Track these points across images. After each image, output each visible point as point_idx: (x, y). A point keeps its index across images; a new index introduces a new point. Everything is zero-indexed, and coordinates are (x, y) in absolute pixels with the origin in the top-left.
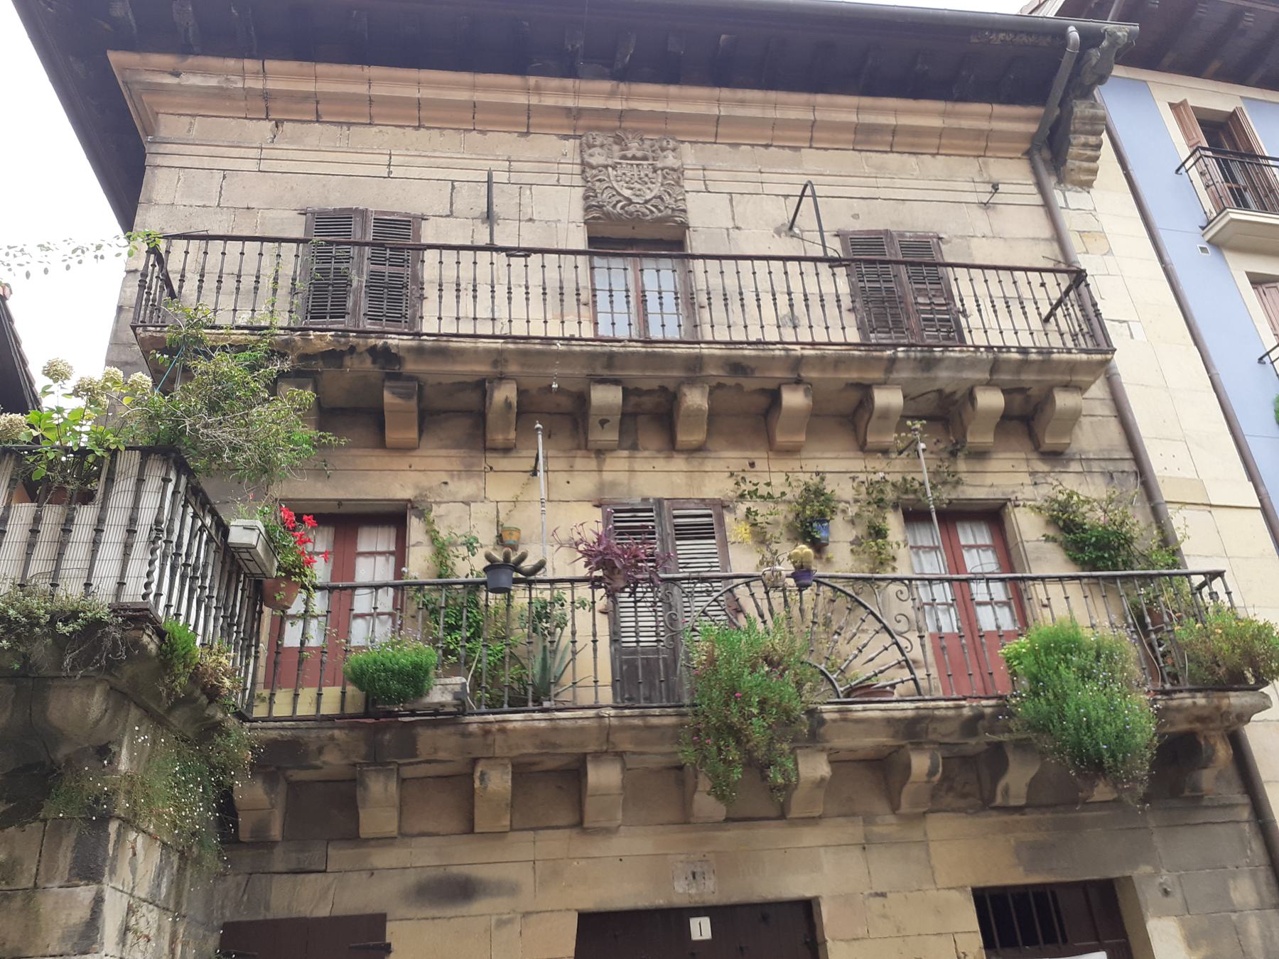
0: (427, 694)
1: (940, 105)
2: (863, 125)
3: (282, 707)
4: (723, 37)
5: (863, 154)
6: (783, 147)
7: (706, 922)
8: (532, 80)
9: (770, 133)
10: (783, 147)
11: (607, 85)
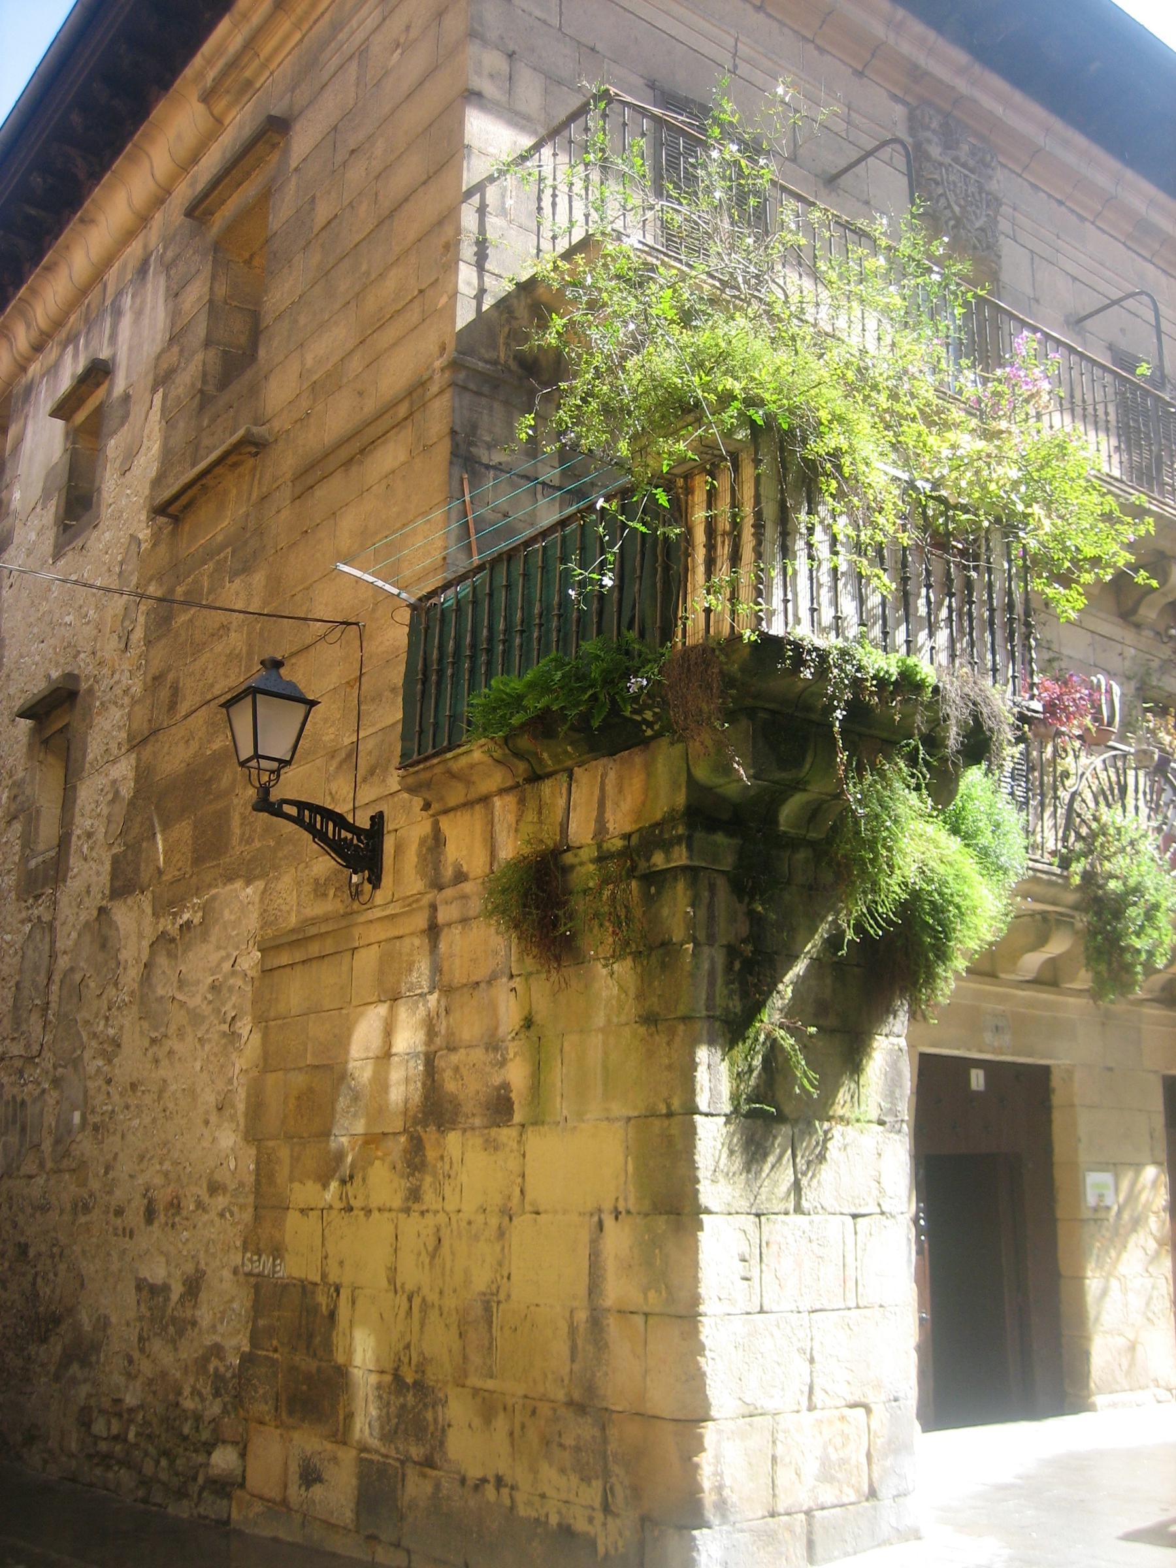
2: (690, 1132)
3: (215, 746)
5: (1130, 253)
6: (1072, 211)
8: (901, 13)
9: (1157, 246)
10: (1072, 211)
11: (961, 57)
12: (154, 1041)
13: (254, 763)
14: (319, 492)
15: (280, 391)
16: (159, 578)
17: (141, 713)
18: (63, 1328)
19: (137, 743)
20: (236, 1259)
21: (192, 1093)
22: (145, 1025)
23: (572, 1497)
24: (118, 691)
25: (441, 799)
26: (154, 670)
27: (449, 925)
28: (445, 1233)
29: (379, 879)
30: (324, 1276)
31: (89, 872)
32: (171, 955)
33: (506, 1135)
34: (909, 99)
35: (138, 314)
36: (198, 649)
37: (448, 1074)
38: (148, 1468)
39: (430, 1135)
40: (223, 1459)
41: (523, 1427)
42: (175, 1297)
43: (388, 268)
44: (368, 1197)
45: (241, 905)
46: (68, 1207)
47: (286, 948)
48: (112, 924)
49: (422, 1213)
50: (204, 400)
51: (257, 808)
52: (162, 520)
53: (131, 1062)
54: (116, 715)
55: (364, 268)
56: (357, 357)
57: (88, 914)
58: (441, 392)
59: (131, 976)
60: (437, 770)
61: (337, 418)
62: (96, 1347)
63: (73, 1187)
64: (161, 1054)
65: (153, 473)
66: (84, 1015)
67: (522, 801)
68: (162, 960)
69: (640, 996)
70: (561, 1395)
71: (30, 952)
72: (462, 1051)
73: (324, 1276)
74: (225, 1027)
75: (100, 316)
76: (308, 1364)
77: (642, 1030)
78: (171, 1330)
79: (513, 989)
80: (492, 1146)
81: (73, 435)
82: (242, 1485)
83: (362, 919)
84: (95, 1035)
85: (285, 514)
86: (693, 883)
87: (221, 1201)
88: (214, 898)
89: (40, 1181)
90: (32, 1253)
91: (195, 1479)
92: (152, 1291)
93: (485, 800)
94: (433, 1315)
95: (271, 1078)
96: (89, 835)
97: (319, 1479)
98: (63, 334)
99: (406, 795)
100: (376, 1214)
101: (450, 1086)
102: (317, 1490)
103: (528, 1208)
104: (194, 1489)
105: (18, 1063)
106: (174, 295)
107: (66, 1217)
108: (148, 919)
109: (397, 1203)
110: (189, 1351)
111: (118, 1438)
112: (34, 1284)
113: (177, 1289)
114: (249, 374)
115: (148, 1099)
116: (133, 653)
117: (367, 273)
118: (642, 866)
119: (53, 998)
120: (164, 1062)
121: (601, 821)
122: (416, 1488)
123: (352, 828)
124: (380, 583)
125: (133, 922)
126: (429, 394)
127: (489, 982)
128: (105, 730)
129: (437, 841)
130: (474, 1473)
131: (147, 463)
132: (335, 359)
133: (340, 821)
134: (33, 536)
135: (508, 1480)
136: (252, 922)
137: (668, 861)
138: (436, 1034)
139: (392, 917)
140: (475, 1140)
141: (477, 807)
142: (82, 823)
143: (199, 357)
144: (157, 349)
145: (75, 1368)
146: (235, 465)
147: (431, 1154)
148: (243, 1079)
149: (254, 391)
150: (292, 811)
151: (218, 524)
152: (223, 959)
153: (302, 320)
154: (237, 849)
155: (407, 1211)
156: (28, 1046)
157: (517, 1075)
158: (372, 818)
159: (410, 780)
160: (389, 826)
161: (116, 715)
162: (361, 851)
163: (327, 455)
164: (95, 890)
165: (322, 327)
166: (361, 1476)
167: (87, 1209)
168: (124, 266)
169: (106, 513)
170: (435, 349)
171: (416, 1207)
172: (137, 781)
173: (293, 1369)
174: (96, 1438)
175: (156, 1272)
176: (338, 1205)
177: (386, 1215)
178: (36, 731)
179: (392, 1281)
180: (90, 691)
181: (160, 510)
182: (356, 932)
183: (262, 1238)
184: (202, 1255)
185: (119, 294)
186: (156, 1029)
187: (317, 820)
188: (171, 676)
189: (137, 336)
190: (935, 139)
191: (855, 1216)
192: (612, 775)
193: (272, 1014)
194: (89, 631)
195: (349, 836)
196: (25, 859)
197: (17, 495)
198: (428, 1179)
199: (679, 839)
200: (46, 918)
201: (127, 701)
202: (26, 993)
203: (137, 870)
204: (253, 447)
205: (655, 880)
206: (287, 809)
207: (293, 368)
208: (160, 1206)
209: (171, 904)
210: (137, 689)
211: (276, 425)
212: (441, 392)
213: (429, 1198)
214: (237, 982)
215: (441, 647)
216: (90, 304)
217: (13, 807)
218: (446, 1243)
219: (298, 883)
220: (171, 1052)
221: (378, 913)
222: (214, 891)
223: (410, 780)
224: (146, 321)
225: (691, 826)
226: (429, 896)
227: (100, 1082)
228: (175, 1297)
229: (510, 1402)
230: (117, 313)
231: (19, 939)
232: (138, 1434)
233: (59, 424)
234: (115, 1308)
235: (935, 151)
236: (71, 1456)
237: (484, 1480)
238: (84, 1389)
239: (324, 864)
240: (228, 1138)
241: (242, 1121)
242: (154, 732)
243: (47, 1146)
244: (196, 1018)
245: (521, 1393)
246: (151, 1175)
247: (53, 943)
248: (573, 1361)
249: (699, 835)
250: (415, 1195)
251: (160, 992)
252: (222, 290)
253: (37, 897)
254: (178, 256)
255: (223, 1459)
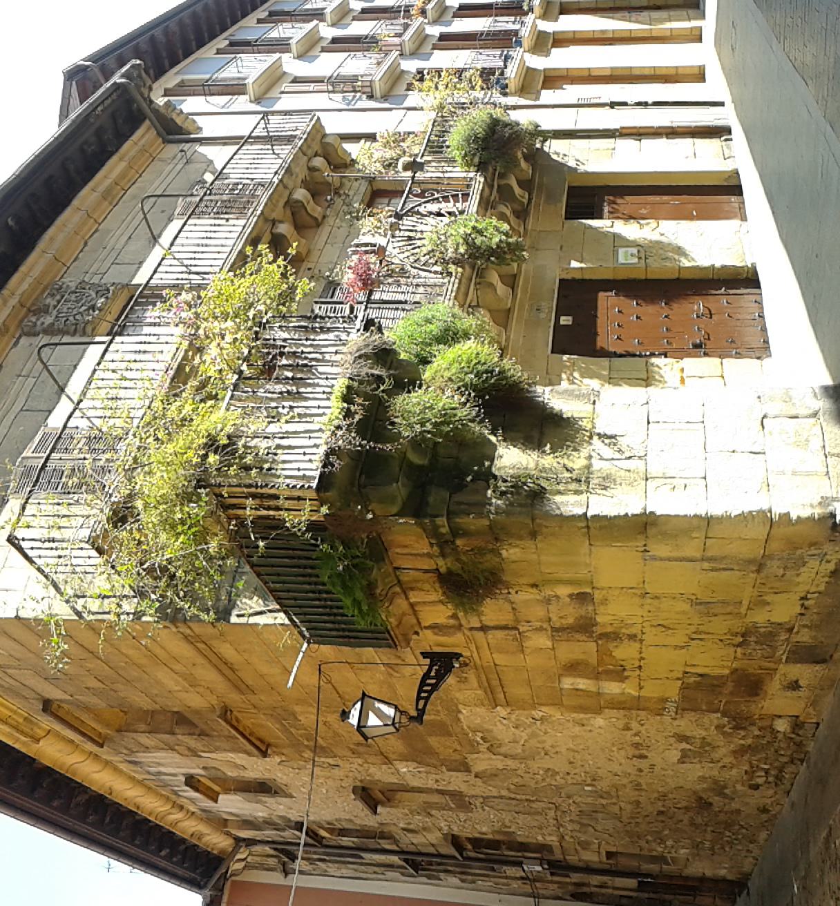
0: (447, 416)
1: (114, 158)
4: (10, 222)
7: (562, 318)
9: (79, 237)
12: (546, 754)
13: (397, 725)
14: (250, 683)
15: (195, 701)
16: (300, 753)
17: (371, 759)
18: (705, 796)
19: (387, 761)
20: (667, 719)
21: (574, 737)
22: (537, 758)
23: (815, 570)
24: (360, 769)
25: (412, 626)
26: (349, 754)
27: (481, 621)
28: (655, 623)
29: (456, 654)
30: (678, 679)
31: (456, 781)
32: (500, 746)
33: (598, 595)
34: (17, 336)
35: (159, 764)
36: (336, 734)
37: (564, 621)
38: (785, 759)
39: (598, 630)
40: (782, 726)
41: (772, 588)
42: (688, 747)
43: (122, 653)
44: (633, 659)
45: (473, 715)
46: (637, 793)
47: (494, 694)
48: (484, 772)
49: (643, 633)
50: (203, 734)
51: (421, 722)
52: (269, 751)
53: (559, 764)
54: (373, 770)
55: (123, 664)
56: (174, 667)
57: (479, 782)
58: (189, 627)
59: (511, 763)
60: (397, 632)
61: (208, 675)
62: (716, 782)
63: (627, 790)
64: (554, 751)
65: (245, 756)
66: (532, 784)
67: (412, 589)
68: (503, 750)
69: (521, 538)
70: (753, 575)
71: (499, 807)
72: (551, 615)
73: (678, 679)
74: (538, 723)
75: (161, 781)
76: (730, 686)
77: (539, 538)
78: (707, 748)
79: (517, 592)
80: (605, 601)
81: (227, 791)
82: (797, 717)
83: (478, 662)
84: (543, 780)
85: (263, 698)
86: (456, 514)
87: (634, 725)
88: (469, 727)
89: (622, 804)
90: (663, 809)
91: (791, 738)
92: (684, 757)
93: (412, 605)
94: (702, 628)
95: (564, 703)
96: (437, 781)
97: (796, 682)
98: (173, 797)
99: (411, 644)
100: (643, 655)
101: (571, 620)
102: (801, 683)
103: (641, 586)
104: (798, 739)
105: (559, 813)
106: (147, 749)
107: (643, 793)
108: (480, 755)
109: (637, 645)
110: (720, 740)
111: (767, 771)
112: (679, 808)
113: (684, 745)
114: (186, 714)
115: (578, 757)
116: (340, 762)
117: (126, 663)
118: (449, 537)
119: (524, 797)
120: (558, 749)
121: (423, 555)
122: (805, 637)
123: (429, 670)
124: (297, 663)
125: (482, 762)
126: (192, 634)
127: (512, 603)
128: (381, 774)
129: (434, 627)
130: (798, 610)
131: (240, 758)
132: (176, 676)
133: (426, 676)
134: (281, 807)
135: (802, 595)
136: (481, 710)
137: (444, 526)
138: (541, 627)
139: (477, 648)
140: (601, 609)
141: (416, 609)
142: (431, 784)
143: (180, 737)
144: (177, 756)
145: (727, 791)
146: (238, 720)
147: (609, 629)
148: (566, 715)
149: (197, 712)
150: (422, 703)
151: (271, 729)
152: (502, 723)
153: (155, 692)
154: (443, 717)
155: (641, 641)
156: (550, 809)
157: (564, 591)
158: (424, 657)
159: (403, 644)
160: (428, 650)
161: (373, 770)
162: (442, 664)
163: (229, 680)
164: (465, 779)
165: (158, 682)
166: (796, 662)
167: (639, 784)
168: (134, 771)
169: (267, 776)
170: (166, 631)
171: (639, 637)
172: (407, 761)
173: (732, 693)
174: (767, 782)
175: (675, 755)
176: (638, 672)
177: (643, 650)
178: (383, 804)
179: (683, 647)
180: (361, 781)
181: (264, 754)
182: (485, 664)
183: (658, 707)
184: (665, 734)
185: (149, 773)
186: (539, 753)
187: (427, 688)
188: (352, 746)
189: (172, 764)
190: (42, 319)
191: (649, 423)
192: (398, 550)
193: (531, 701)
194: (330, 782)
195: (434, 671)
196: (451, 809)
197: (260, 814)
198: (623, 630)
199: (433, 522)
200: (481, 800)
201: (365, 765)
202: (522, 809)
203: (456, 761)
204: (226, 713)
205: (456, 532)
206: (420, 707)
207: (183, 695)
208: (637, 753)
209: (473, 746)
210: (360, 761)
211: (215, 702)
212: (189, 627)
213: (633, 631)
214: (513, 717)
215: (330, 630)
216: (156, 785)
217: (424, 814)
218: (661, 623)
219: (460, 690)
220: (552, 746)
221: (475, 655)
222: (465, 727)
223: (403, 644)
224: (162, 761)
225: (425, 516)
226: (466, 632)
227: (569, 777)
228: (688, 747)
229: (756, 593)
230: (159, 773)
231: (492, 812)
232: (765, 764)
233: (221, 797)
234: (694, 774)
235: (49, 320)
236: (776, 793)
237: (802, 605)
238: (739, 787)
239: (451, 680)
240: (599, 721)
241: (590, 715)
242: (382, 754)
243: (604, 802)
244: (533, 735)
245: (751, 589)
246: (620, 756)
247: (494, 797)
248: (733, 569)
249: (429, 511)
250: (632, 637)
251: (520, 751)
252: (143, 727)
253: (470, 804)
254: (126, 748)
255: (782, 726)
